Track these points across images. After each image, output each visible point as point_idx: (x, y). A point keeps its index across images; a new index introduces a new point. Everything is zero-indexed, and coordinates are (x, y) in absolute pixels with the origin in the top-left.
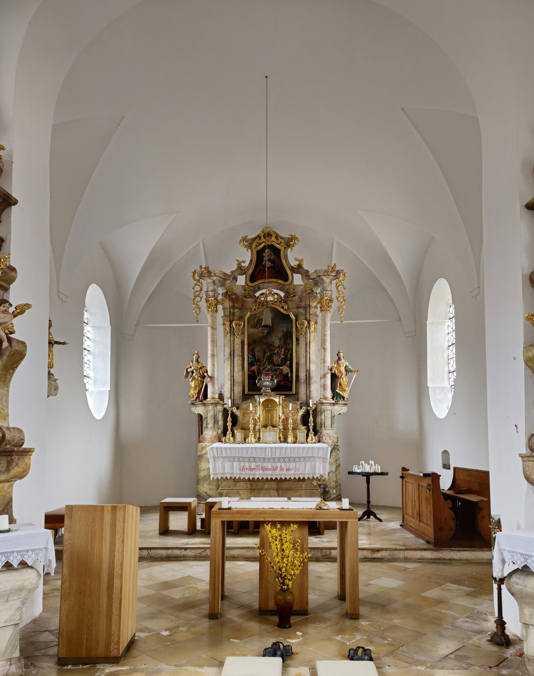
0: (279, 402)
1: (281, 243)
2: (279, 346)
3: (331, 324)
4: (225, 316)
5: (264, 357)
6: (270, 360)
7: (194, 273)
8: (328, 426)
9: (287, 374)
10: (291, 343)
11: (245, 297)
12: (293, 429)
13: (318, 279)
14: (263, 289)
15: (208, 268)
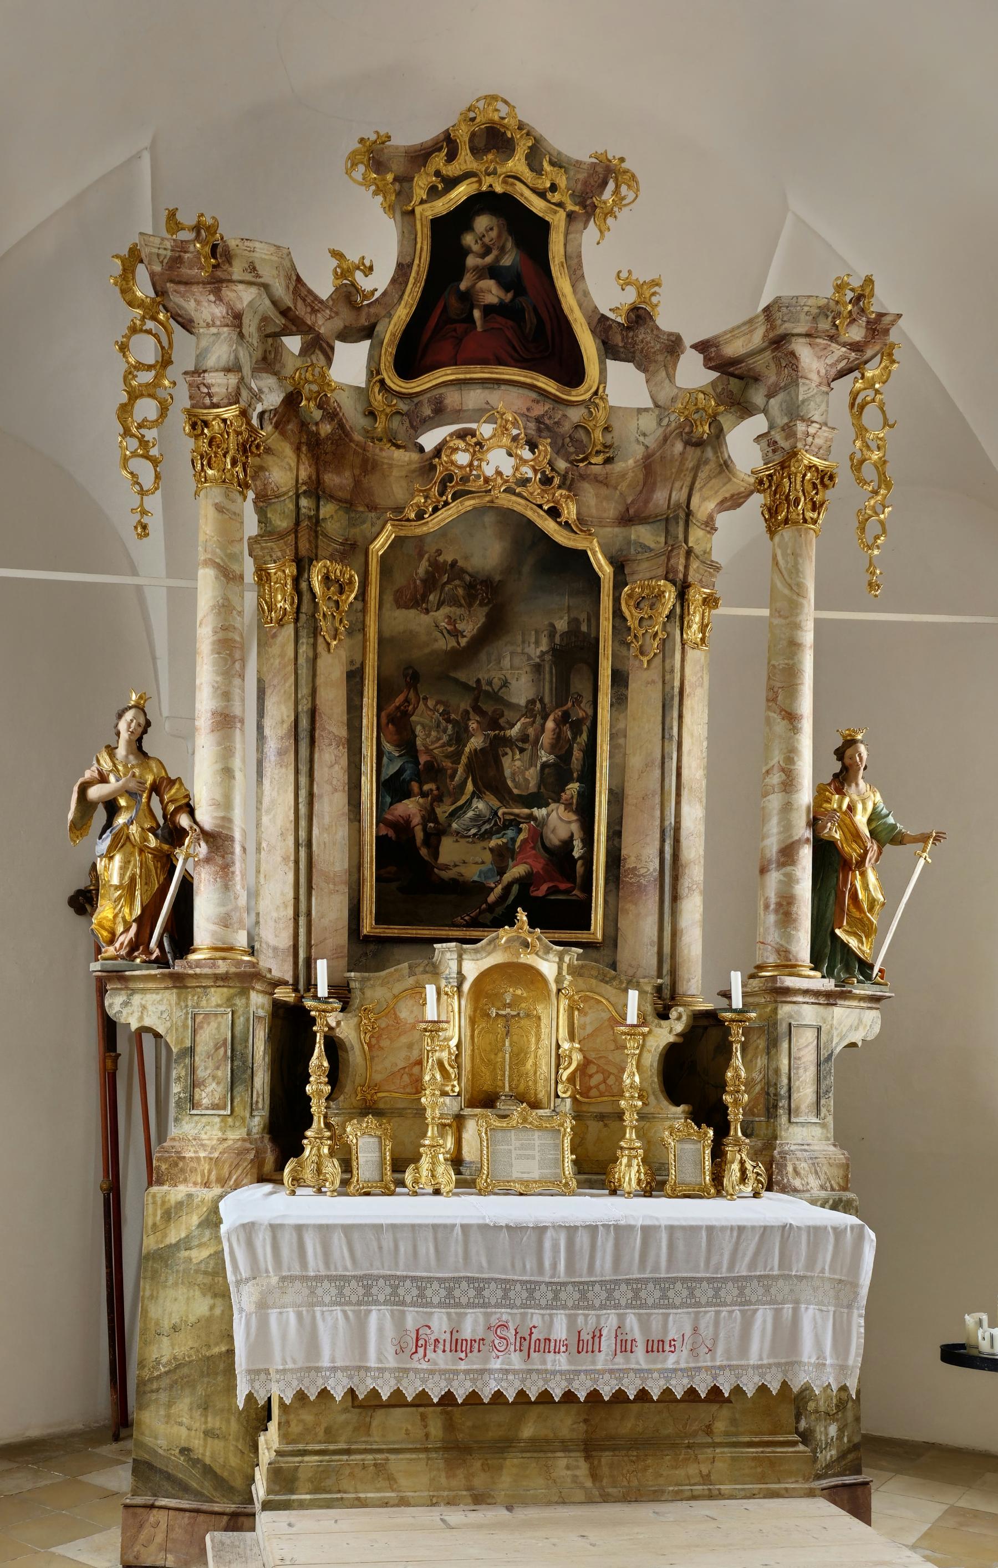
0: (559, 980)
1: (554, 188)
2: (532, 702)
4: (267, 531)
7: (133, 258)
9: (568, 844)
10: (587, 696)
15: (212, 229)
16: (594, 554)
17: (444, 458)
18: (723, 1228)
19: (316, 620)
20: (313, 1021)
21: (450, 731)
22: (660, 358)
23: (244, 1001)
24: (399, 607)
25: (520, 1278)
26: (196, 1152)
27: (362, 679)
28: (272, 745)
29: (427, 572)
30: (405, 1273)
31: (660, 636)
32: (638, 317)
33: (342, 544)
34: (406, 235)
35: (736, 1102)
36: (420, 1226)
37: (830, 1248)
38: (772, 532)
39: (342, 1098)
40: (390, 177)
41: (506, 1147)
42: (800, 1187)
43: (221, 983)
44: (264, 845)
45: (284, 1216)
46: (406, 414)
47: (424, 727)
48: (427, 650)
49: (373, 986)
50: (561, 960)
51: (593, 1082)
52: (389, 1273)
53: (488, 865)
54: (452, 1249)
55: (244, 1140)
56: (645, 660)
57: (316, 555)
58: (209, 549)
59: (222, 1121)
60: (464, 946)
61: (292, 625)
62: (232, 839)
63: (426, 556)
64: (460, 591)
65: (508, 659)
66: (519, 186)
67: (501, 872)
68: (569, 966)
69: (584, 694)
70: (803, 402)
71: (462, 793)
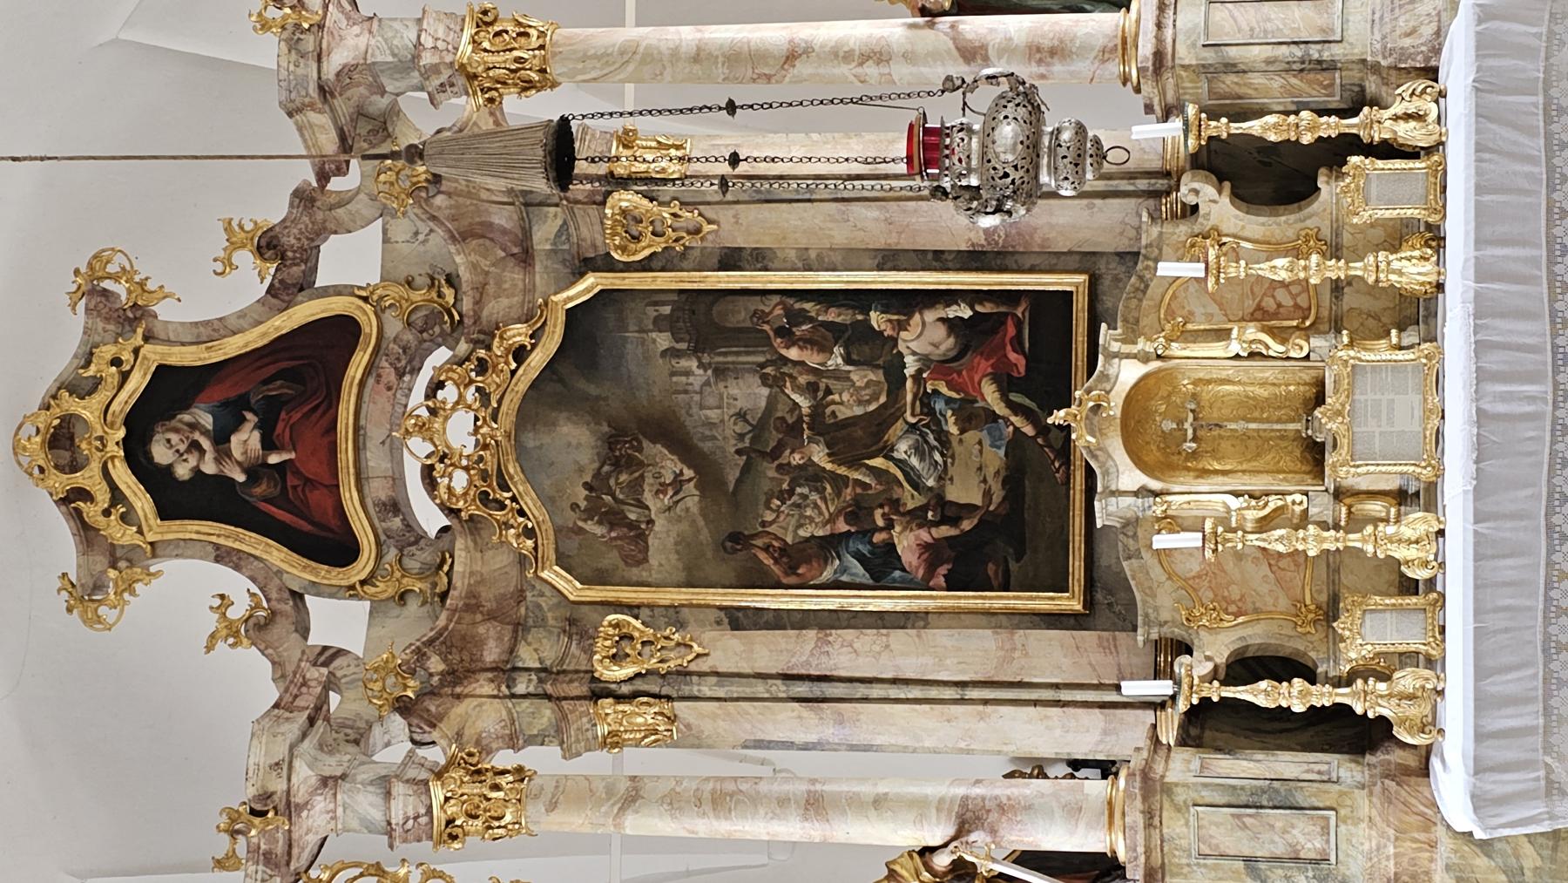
0: (1144, 358)
1: (116, 362)
2: (765, 380)
3: (639, 23)
4: (558, 734)
5: (839, 482)
6: (858, 439)
8: (1321, 21)
9: (952, 325)
10: (755, 304)
11: (444, 596)
12: (1334, 251)
13: (343, 106)
14: (398, 480)
15: (233, 816)
16: (570, 299)
17: (461, 504)
18: (1479, 173)
19: (669, 673)
20: (1205, 701)
21: (805, 490)
22: (320, 216)
23: (1179, 790)
24: (646, 560)
25: (1548, 444)
26: (1388, 859)
27: (739, 609)
28: (830, 732)
29: (600, 523)
30: (1541, 598)
31: (676, 210)
32: (269, 246)
33: (570, 637)
34: (180, 551)
35: (1312, 128)
36: (1476, 578)
37: (1506, 26)
38: (554, 85)
39: (1313, 654)
40: (112, 574)
41: (1377, 440)
42: (1434, 26)
43: (1156, 821)
44: (962, 745)
45: (1464, 756)
46: (401, 550)
47: (800, 526)
48: (701, 522)
49: (1156, 609)
50: (1117, 355)
51: (1288, 302)
52: (1540, 619)
53: (984, 435)
54: (1508, 535)
55: (1371, 793)
56: (707, 228)
57: (586, 672)
58: (602, 821)
59: (1345, 822)
60: (1099, 489)
61: (676, 704)
62: (965, 799)
63: (580, 524)
64: (623, 477)
65: (708, 412)
66: (115, 407)
67: (993, 417)
68: (1124, 341)
69: (753, 308)
70: (394, 55)
71: (887, 472)
